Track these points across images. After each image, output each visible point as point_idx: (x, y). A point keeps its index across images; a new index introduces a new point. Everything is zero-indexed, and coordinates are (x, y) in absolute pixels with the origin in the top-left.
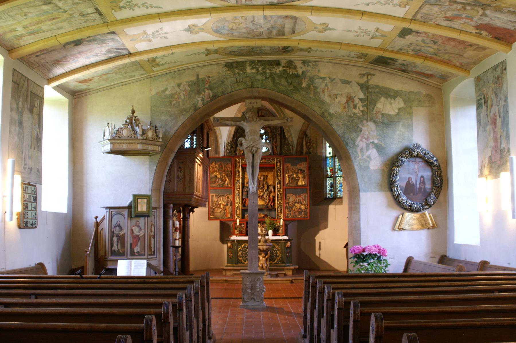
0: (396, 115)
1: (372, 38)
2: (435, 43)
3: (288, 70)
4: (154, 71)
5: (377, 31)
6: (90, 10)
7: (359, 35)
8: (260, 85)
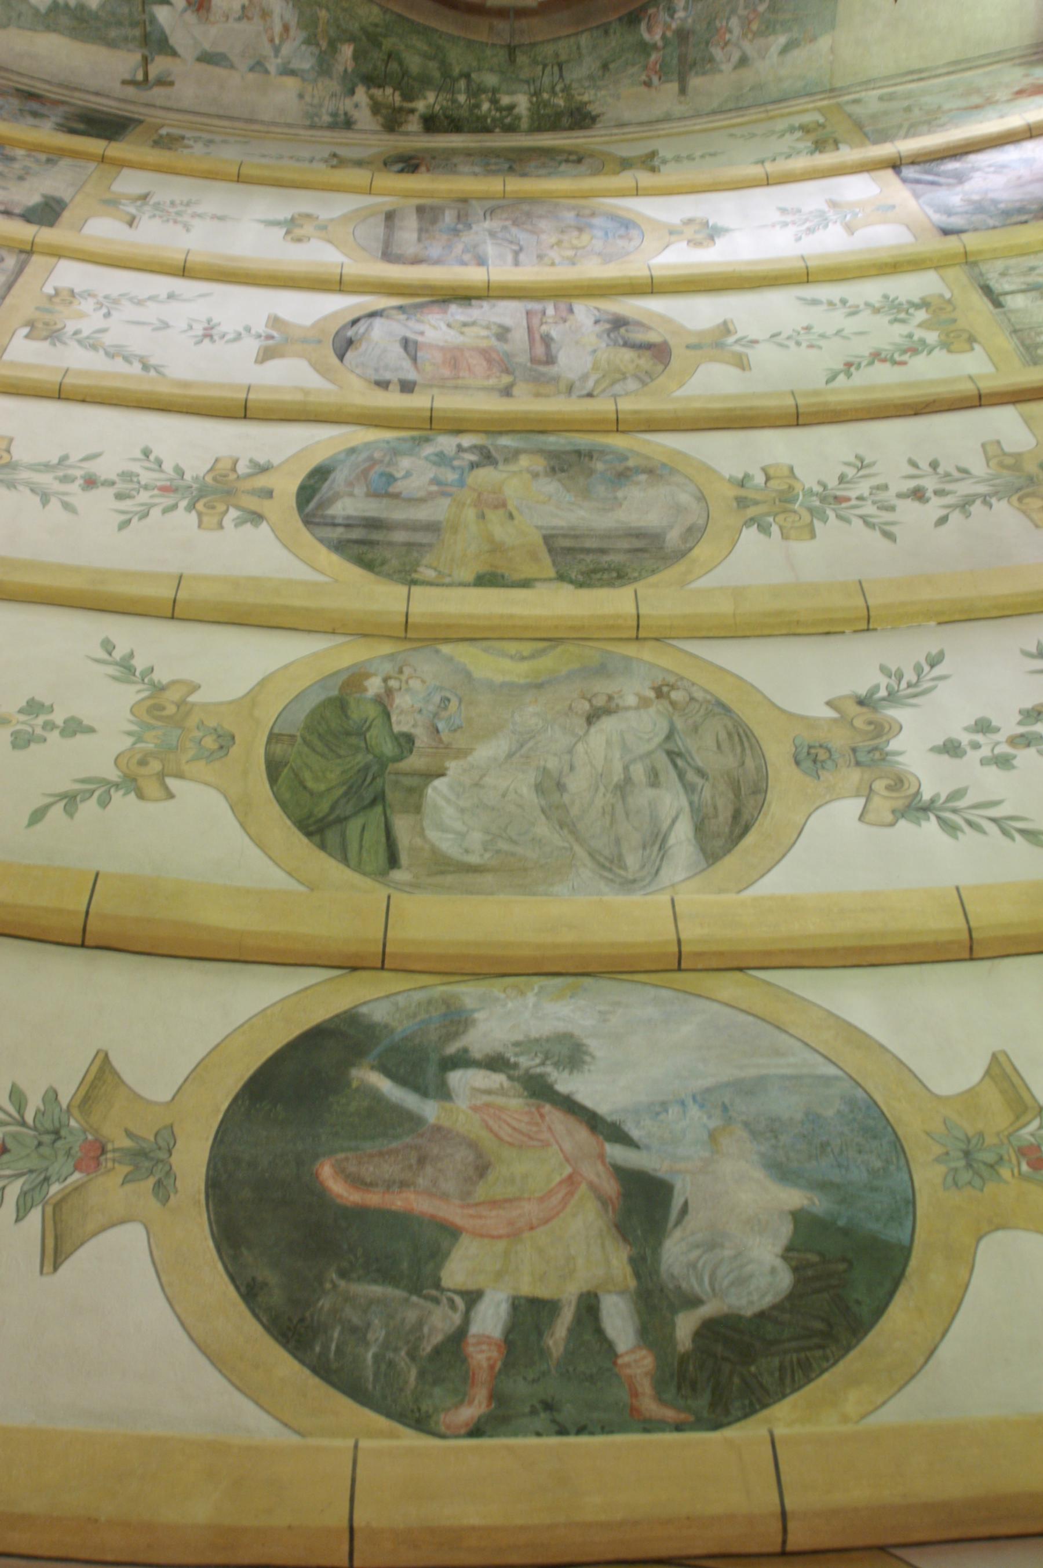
1: (145, 197)
3: (398, 98)
4: (819, 110)
5: (133, 218)
6: (1017, 302)
7: (188, 204)
8: (489, 52)
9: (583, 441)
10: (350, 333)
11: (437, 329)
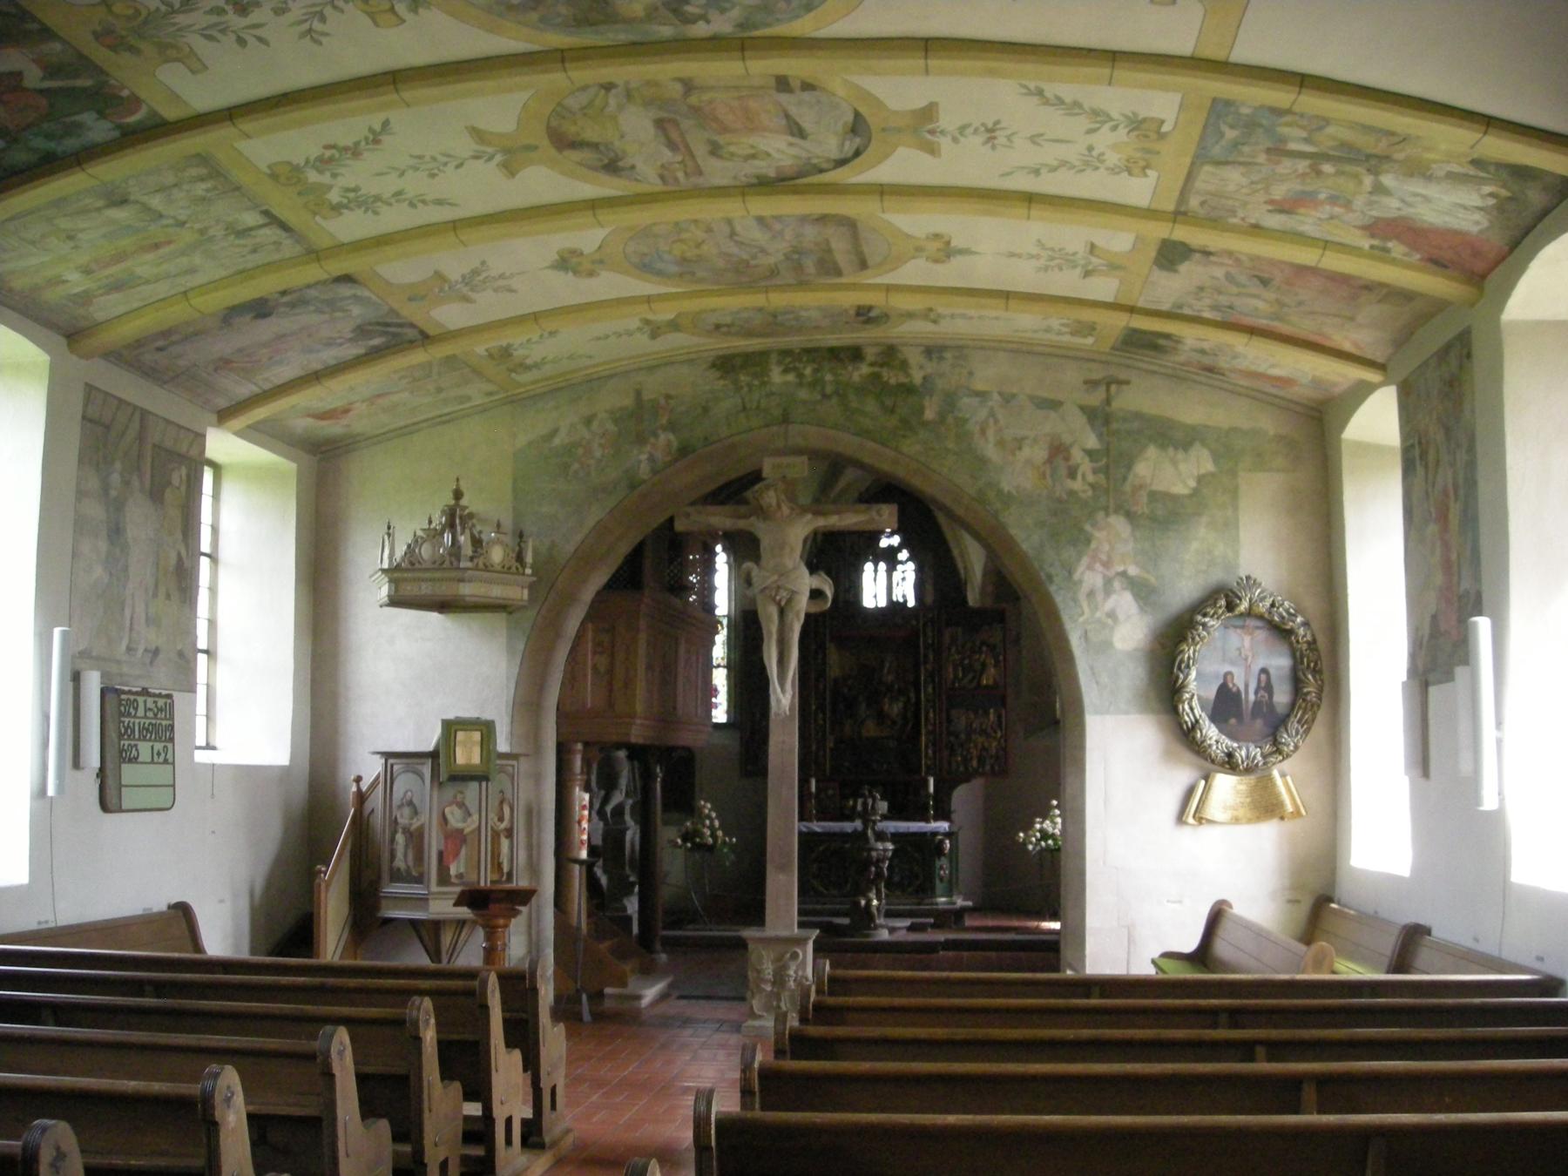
0: (1191, 496)
2: (1265, 282)
6: (251, 219)
7: (1046, 269)
11: (779, 151)
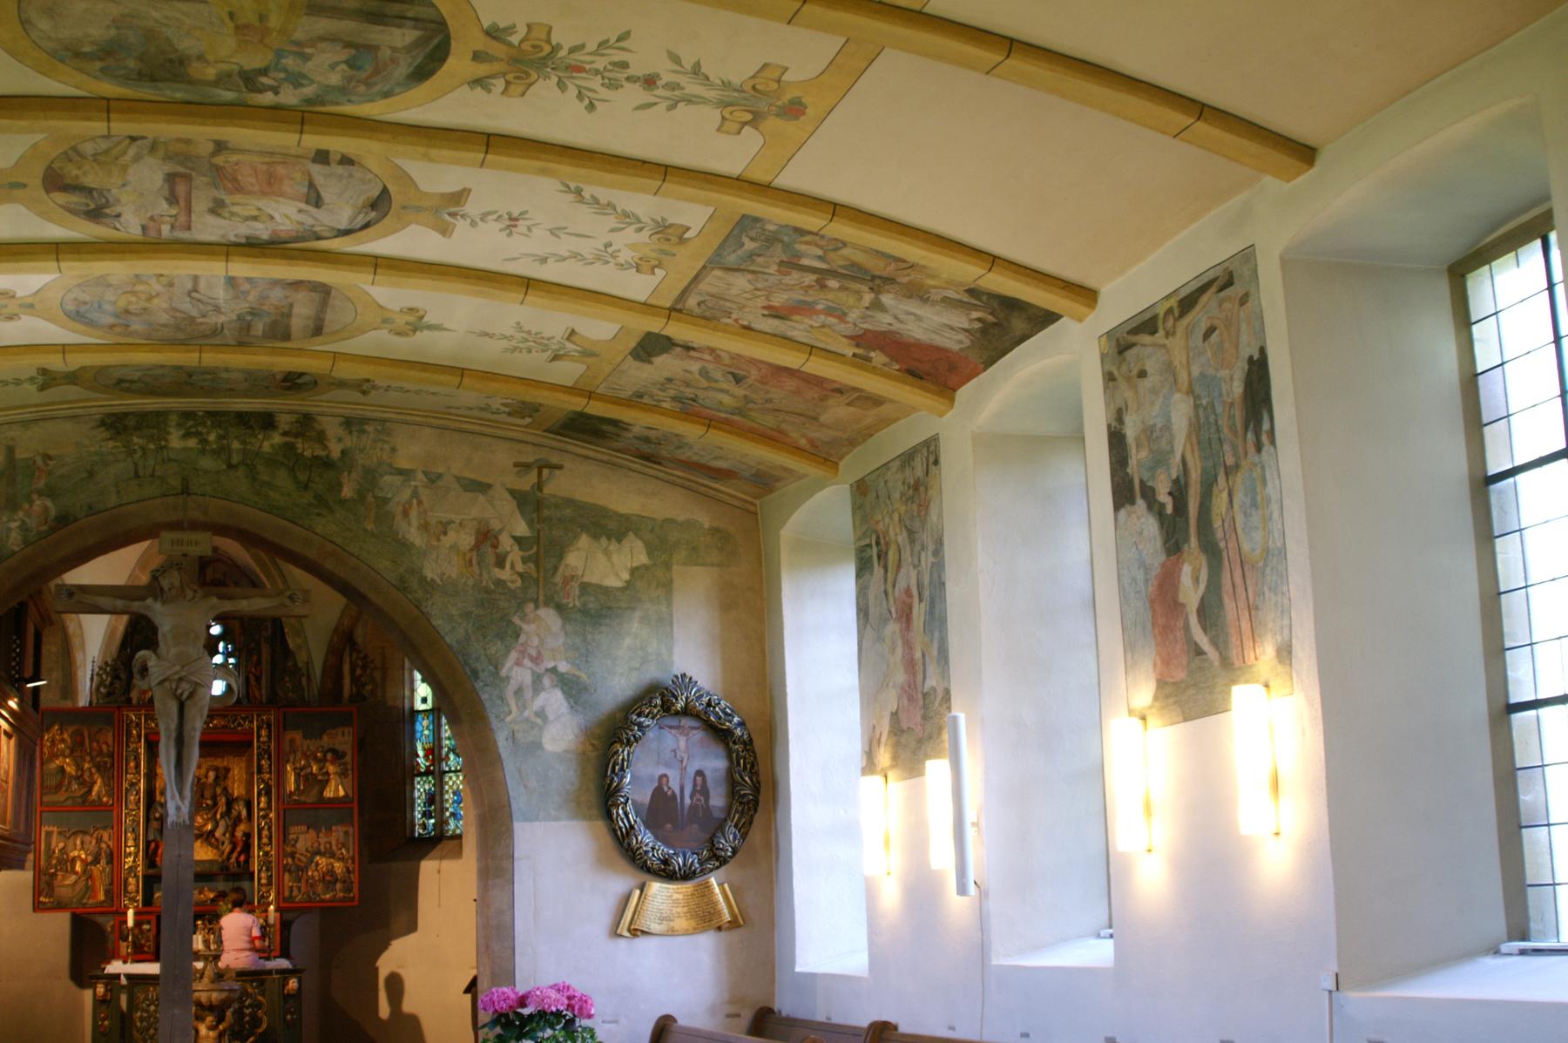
0: (623, 589)
1: (556, 358)
2: (738, 380)
3: (300, 446)
7: (515, 349)
9: (146, 92)
10: (373, 214)
11: (285, 215)
